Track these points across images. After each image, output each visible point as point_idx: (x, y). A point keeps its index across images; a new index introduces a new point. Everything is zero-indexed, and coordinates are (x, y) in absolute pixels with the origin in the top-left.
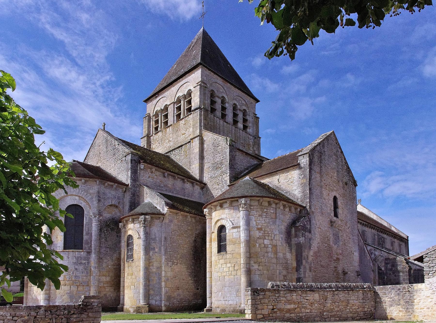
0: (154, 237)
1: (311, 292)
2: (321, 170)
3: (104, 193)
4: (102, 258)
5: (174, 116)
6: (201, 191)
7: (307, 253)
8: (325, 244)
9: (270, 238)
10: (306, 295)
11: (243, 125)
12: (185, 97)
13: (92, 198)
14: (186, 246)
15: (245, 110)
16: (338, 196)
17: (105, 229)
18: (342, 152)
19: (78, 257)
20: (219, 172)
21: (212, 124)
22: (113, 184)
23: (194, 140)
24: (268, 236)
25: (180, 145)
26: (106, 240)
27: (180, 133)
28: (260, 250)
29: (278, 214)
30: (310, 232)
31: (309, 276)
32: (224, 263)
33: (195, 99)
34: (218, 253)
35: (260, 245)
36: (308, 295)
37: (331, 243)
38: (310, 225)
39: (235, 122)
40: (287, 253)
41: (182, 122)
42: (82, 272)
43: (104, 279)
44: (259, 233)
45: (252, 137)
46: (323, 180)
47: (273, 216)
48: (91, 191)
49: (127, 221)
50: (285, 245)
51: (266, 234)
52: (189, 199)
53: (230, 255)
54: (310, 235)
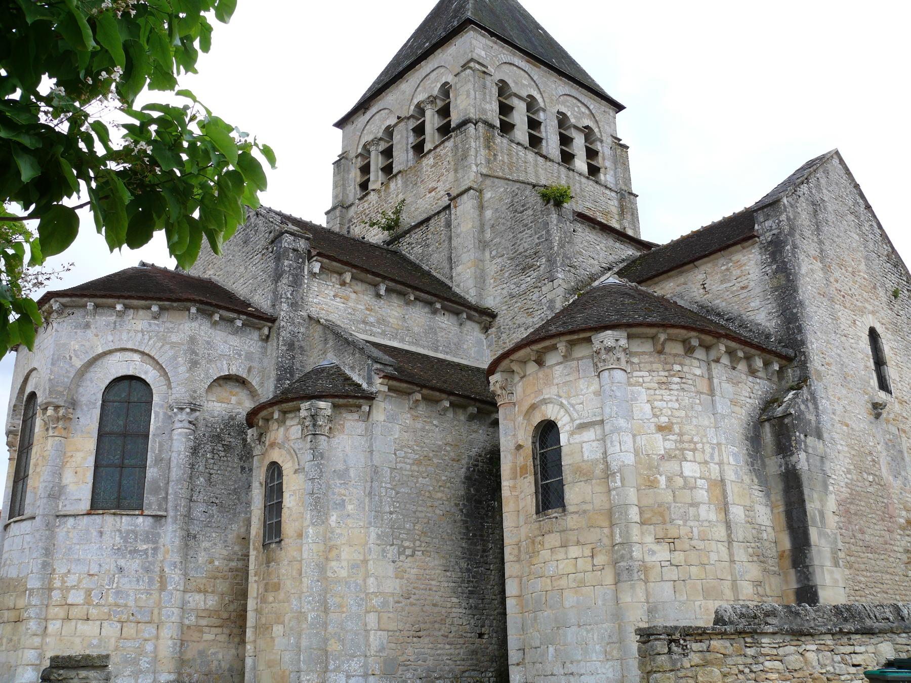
0: (340, 466)
1: (865, 638)
2: (822, 251)
3: (208, 343)
4: (195, 537)
5: (407, 151)
6: (483, 337)
7: (817, 505)
8: (869, 474)
9: (699, 457)
10: (849, 649)
11: (589, 164)
12: (432, 100)
13: (175, 358)
14: (440, 495)
15: (587, 127)
16: (880, 329)
17: (208, 447)
18: (868, 207)
19: (128, 532)
20: (529, 280)
21: (506, 160)
22: (235, 315)
23: (458, 200)
24: (694, 450)
25: (425, 216)
26: (209, 480)
27: (422, 189)
28: (671, 498)
29: (716, 381)
30: (819, 436)
31: (836, 581)
32: (558, 544)
33: (459, 101)
34: (538, 512)
35: (669, 479)
36: (858, 649)
37: (884, 472)
38: (817, 416)
39: (567, 158)
40: (758, 507)
41: (429, 161)
42: (138, 581)
43: (197, 600)
44: (665, 440)
45: (613, 194)
46: (832, 280)
47: (703, 385)
48: (174, 338)
49: (267, 420)
50: (747, 479)
51: (686, 445)
52: (449, 358)
53: (575, 516)
54: (819, 445)
